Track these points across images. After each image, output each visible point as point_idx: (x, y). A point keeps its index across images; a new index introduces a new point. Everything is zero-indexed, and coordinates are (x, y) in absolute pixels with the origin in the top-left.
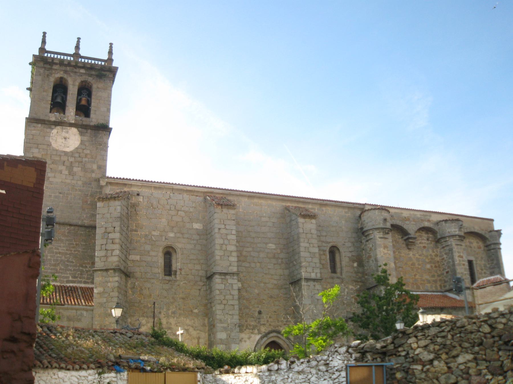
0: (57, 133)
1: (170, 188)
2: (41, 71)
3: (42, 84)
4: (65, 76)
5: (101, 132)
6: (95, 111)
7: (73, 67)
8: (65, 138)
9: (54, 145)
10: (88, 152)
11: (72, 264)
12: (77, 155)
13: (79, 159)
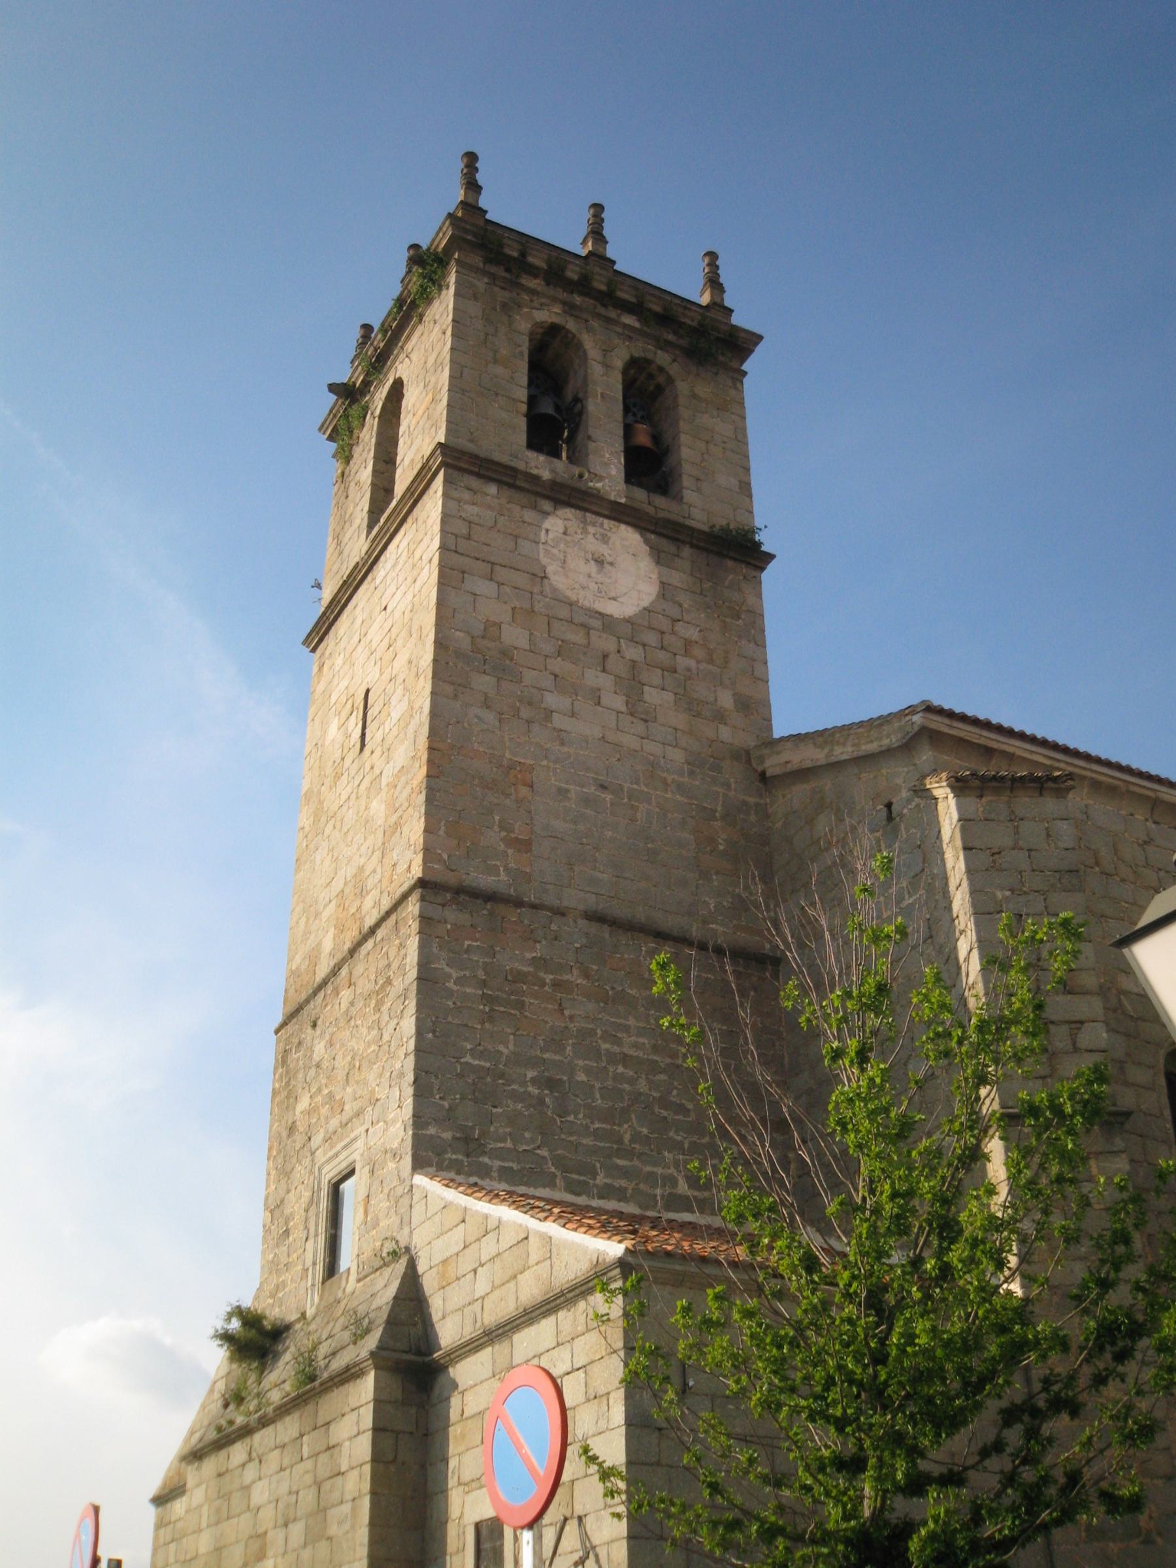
0: (565, 533)
1: (1148, 798)
2: (478, 283)
3: (487, 334)
4: (571, 325)
5: (730, 563)
6: (698, 480)
7: (596, 299)
8: (600, 562)
9: (558, 579)
10: (693, 633)
11: (680, 1117)
12: (651, 638)
13: (662, 656)
